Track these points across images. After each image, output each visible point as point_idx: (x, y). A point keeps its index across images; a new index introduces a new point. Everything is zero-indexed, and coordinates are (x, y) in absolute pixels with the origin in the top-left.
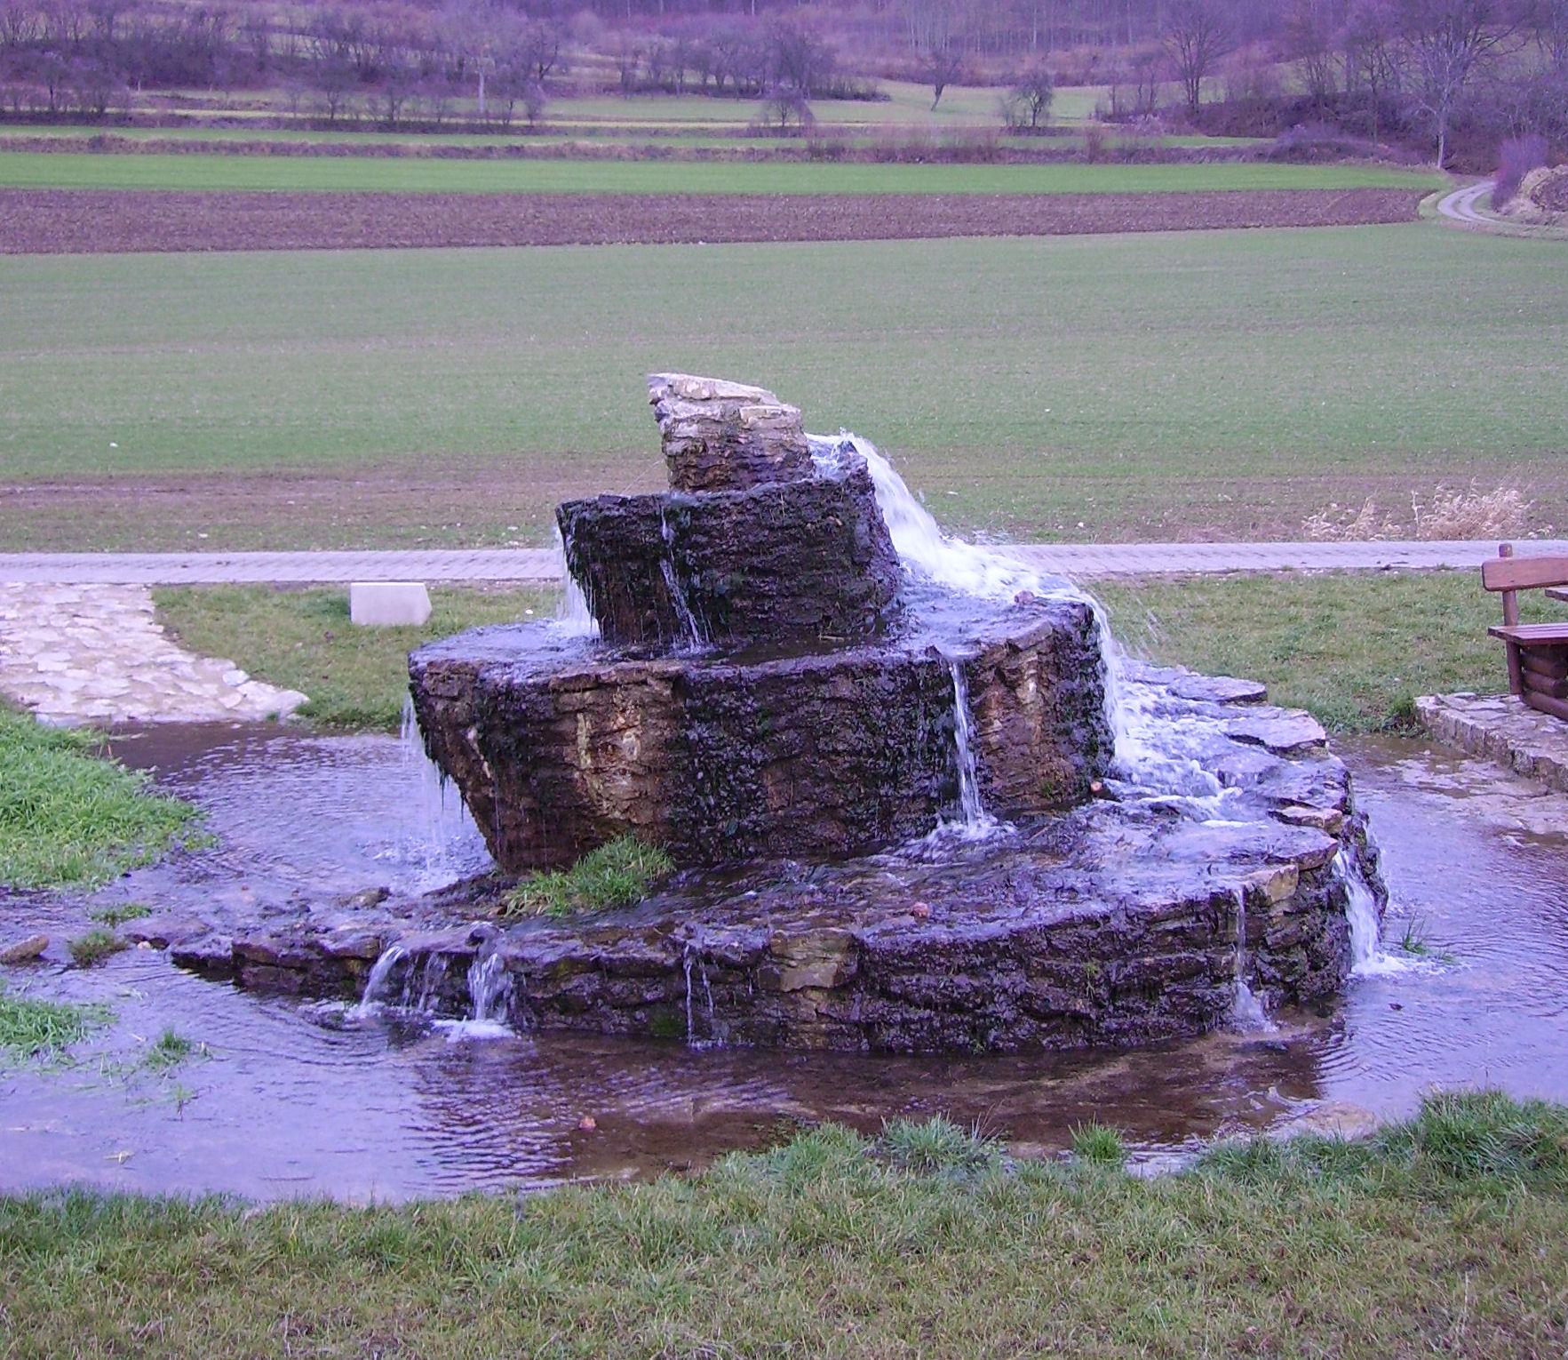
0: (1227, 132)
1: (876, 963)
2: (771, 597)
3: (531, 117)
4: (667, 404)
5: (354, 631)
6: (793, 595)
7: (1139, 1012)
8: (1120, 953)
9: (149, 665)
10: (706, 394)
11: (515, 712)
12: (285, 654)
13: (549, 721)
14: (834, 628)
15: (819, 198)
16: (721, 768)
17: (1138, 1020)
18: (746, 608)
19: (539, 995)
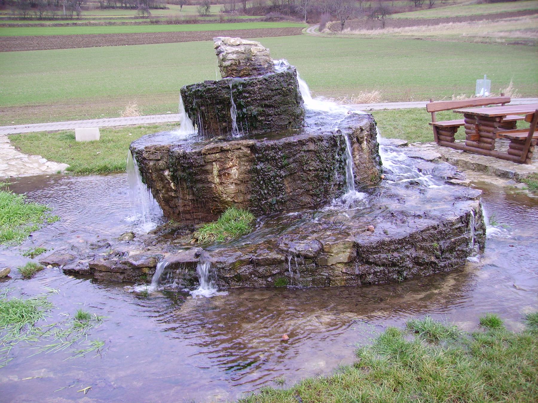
0: (253, 15)
1: (364, 252)
2: (271, 116)
3: (78, 16)
4: (223, 48)
5: (78, 144)
6: (279, 114)
7: (449, 259)
8: (443, 238)
9: (13, 159)
10: (238, 43)
11: (188, 163)
12: (57, 152)
13: (202, 166)
14: (292, 126)
15: (154, 33)
16: (269, 179)
17: (449, 261)
18: (263, 120)
19: (228, 276)
